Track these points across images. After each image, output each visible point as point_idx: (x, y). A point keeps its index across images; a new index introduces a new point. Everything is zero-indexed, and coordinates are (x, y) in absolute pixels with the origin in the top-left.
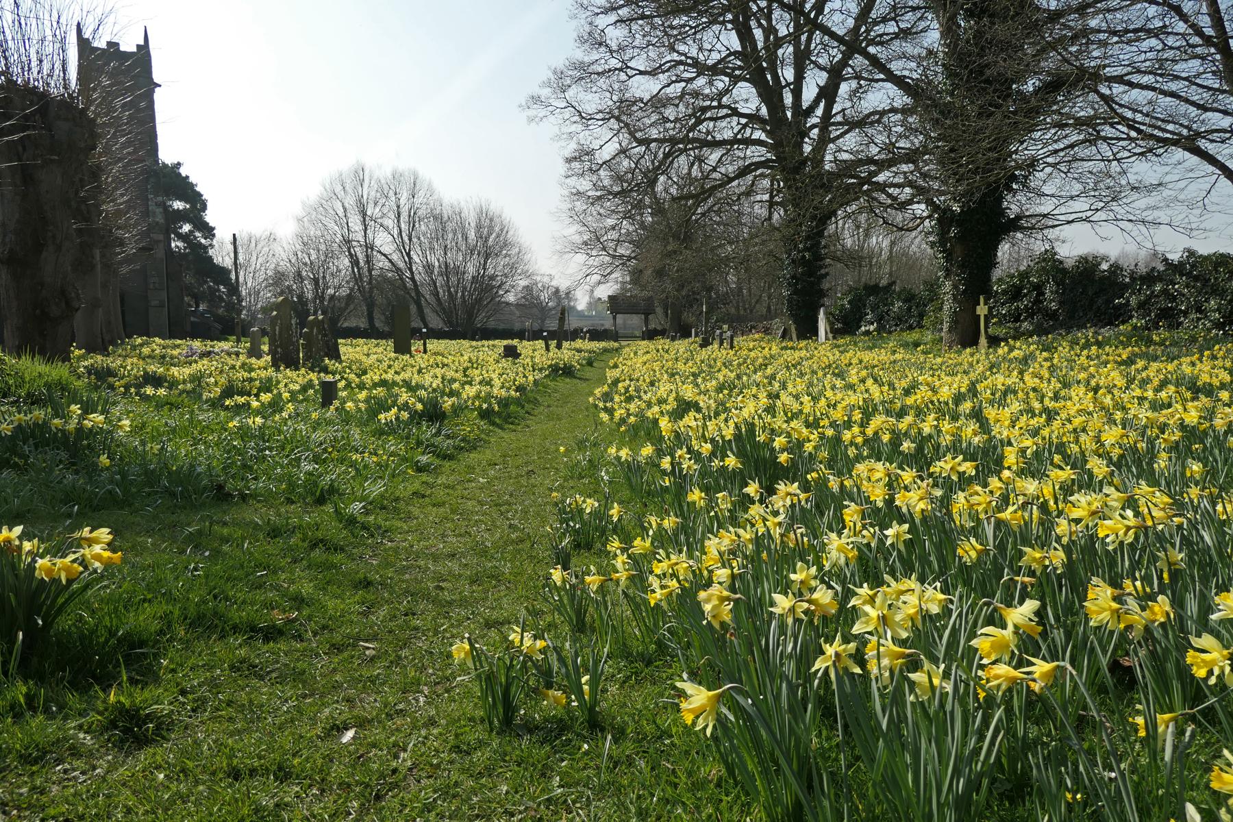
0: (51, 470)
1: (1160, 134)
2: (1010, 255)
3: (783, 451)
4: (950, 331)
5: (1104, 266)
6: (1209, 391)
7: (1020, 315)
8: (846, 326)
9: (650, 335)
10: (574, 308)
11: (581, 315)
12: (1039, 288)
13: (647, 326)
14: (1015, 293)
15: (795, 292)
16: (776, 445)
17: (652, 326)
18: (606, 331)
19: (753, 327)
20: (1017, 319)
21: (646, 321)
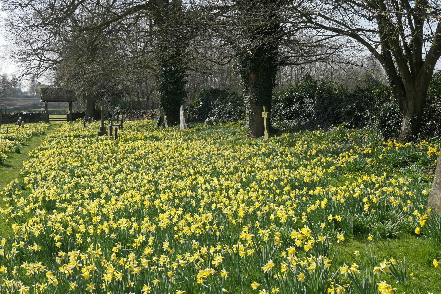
0: (183, 31)
1: (12, 107)
2: (288, 75)
3: (58, 241)
4: (250, 126)
5: (388, 69)
6: (204, 227)
7: (292, 115)
8: (197, 117)
9: (72, 118)
10: (19, 90)
11: (25, 96)
12: (301, 99)
13: (70, 110)
14: (289, 102)
15: (167, 93)
16: (56, 239)
17: (75, 110)
18: (39, 114)
19: (145, 113)
20: (290, 118)
21: (70, 107)
